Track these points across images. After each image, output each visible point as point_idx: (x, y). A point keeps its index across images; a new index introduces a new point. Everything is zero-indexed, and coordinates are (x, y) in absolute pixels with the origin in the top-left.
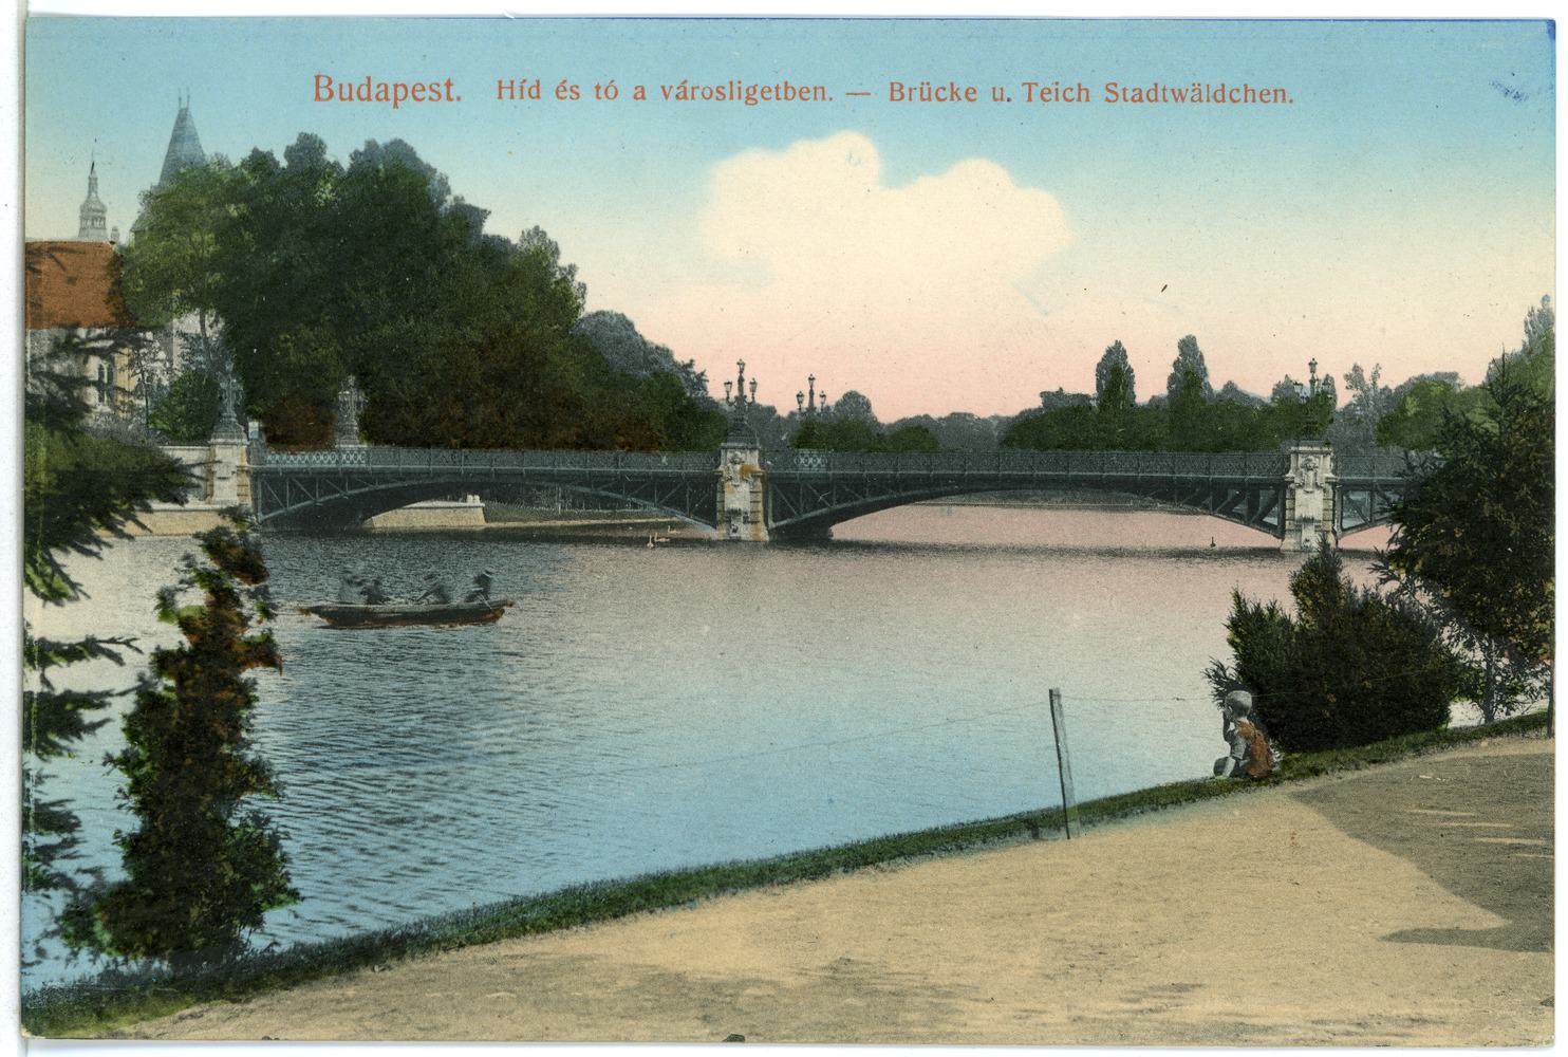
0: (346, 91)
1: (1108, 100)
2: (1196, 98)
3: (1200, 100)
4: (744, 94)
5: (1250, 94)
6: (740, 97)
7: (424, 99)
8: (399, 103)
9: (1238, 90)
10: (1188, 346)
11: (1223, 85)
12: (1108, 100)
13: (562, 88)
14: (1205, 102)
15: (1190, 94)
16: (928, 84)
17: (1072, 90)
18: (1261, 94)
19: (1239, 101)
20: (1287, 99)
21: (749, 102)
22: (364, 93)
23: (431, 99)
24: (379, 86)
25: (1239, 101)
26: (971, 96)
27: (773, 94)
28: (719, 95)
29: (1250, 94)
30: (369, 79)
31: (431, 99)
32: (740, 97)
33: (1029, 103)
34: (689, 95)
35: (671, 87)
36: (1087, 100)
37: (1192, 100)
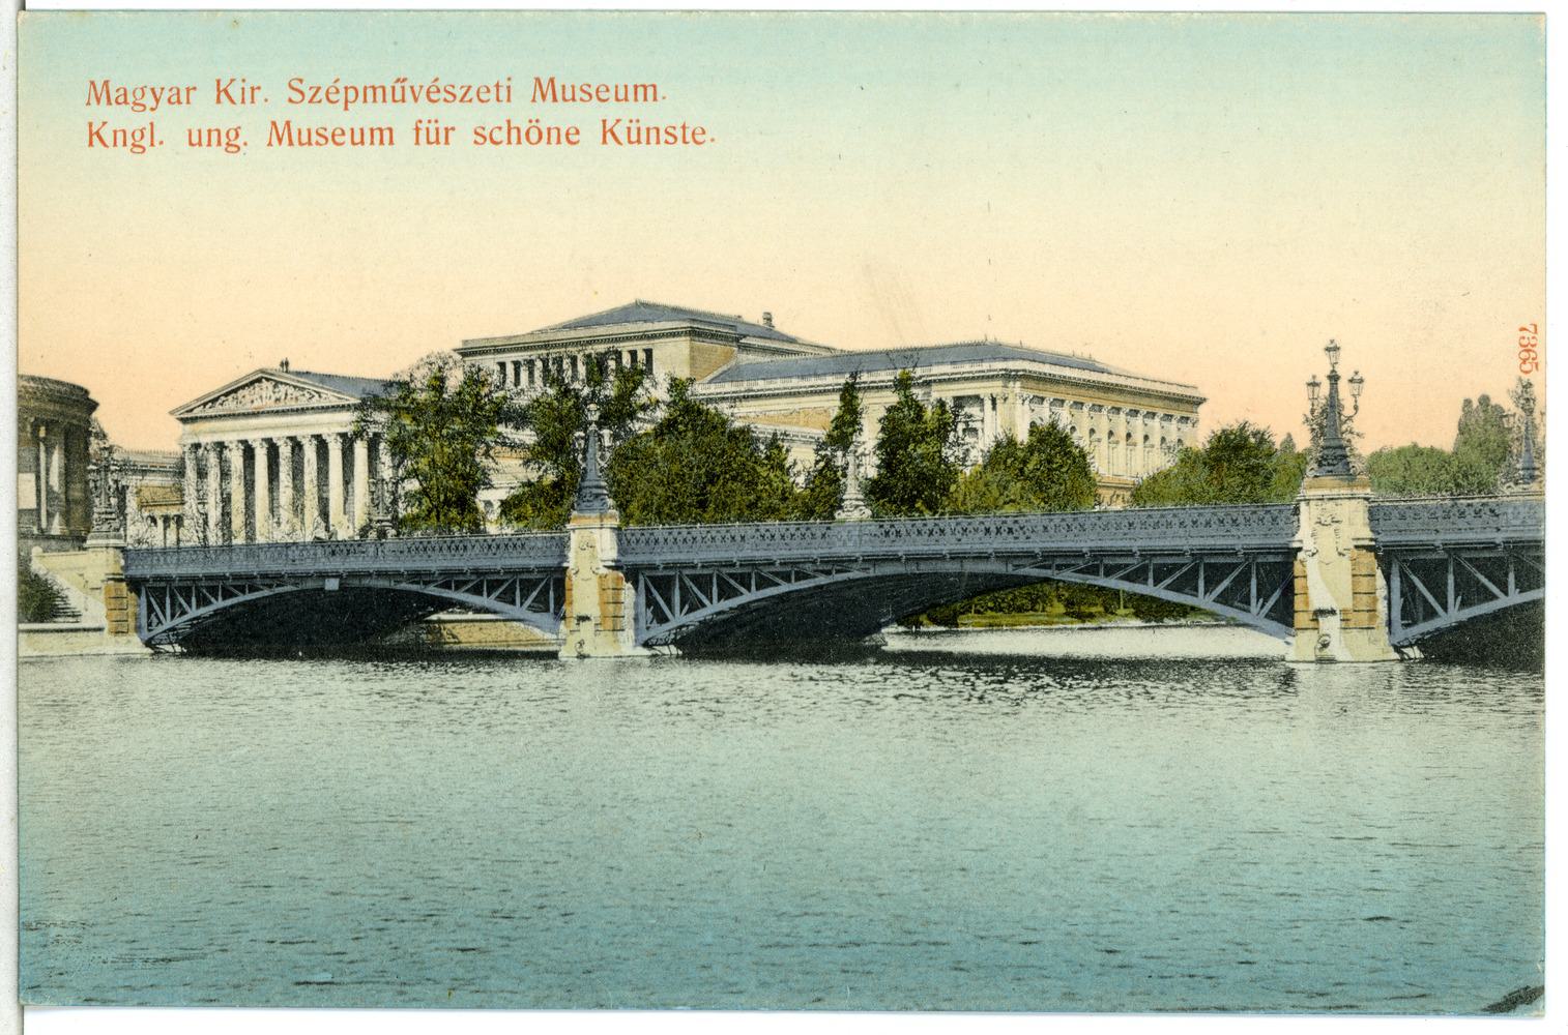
0: (214, 140)
1: (476, 142)
2: (174, 99)
3: (179, 102)
4: (224, 140)
5: (514, 133)
6: (125, 144)
7: (337, 101)
8: (349, 105)
9: (500, 128)
10: (1289, 435)
11: (346, 109)
12: (476, 142)
13: (333, 90)
14: (505, 103)
15: (166, 94)
16: (436, 121)
17: (500, 128)
18: (567, 134)
19: (501, 142)
20: (659, 97)
21: (230, 149)
22: (351, 93)
23: (445, 100)
24: (118, 90)
25: (501, 142)
26: (573, 138)
27: (493, 96)
28: (589, 90)
29: (514, 133)
30: (346, 109)
31: (445, 100)
32: (125, 144)
33: (604, 118)
34: (183, 98)
35: (163, 89)
36: (391, 142)
37: (169, 101)
